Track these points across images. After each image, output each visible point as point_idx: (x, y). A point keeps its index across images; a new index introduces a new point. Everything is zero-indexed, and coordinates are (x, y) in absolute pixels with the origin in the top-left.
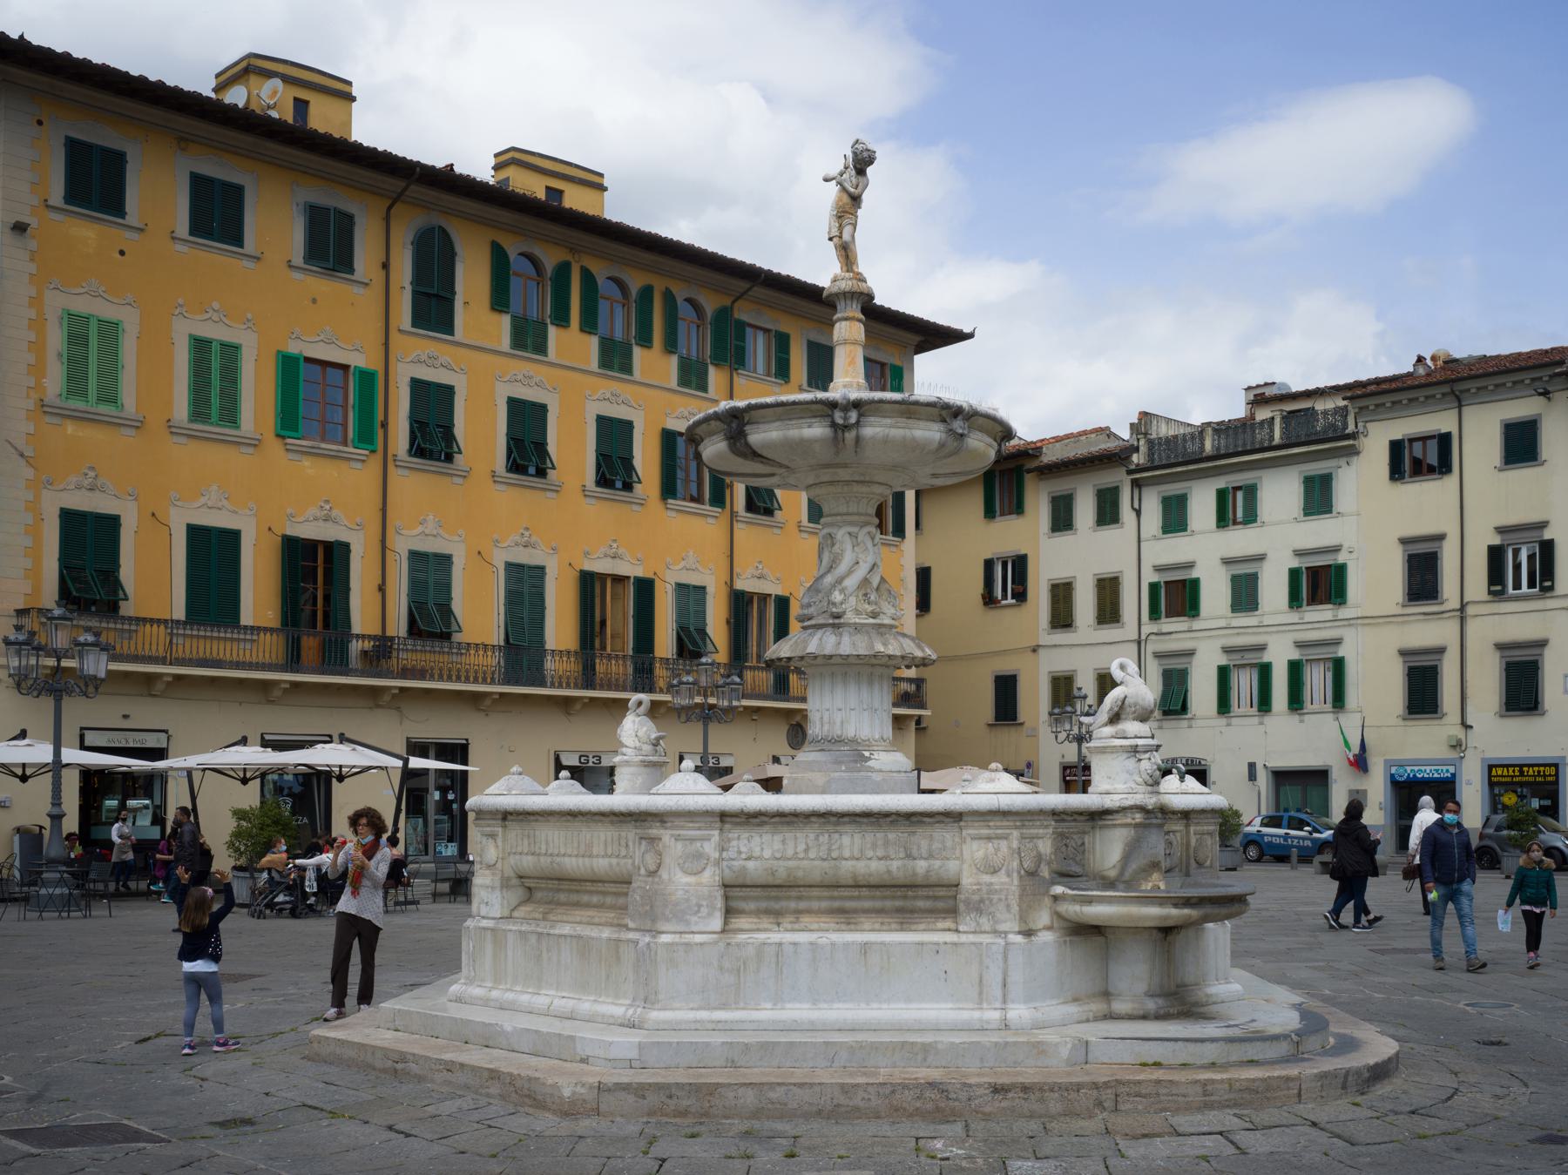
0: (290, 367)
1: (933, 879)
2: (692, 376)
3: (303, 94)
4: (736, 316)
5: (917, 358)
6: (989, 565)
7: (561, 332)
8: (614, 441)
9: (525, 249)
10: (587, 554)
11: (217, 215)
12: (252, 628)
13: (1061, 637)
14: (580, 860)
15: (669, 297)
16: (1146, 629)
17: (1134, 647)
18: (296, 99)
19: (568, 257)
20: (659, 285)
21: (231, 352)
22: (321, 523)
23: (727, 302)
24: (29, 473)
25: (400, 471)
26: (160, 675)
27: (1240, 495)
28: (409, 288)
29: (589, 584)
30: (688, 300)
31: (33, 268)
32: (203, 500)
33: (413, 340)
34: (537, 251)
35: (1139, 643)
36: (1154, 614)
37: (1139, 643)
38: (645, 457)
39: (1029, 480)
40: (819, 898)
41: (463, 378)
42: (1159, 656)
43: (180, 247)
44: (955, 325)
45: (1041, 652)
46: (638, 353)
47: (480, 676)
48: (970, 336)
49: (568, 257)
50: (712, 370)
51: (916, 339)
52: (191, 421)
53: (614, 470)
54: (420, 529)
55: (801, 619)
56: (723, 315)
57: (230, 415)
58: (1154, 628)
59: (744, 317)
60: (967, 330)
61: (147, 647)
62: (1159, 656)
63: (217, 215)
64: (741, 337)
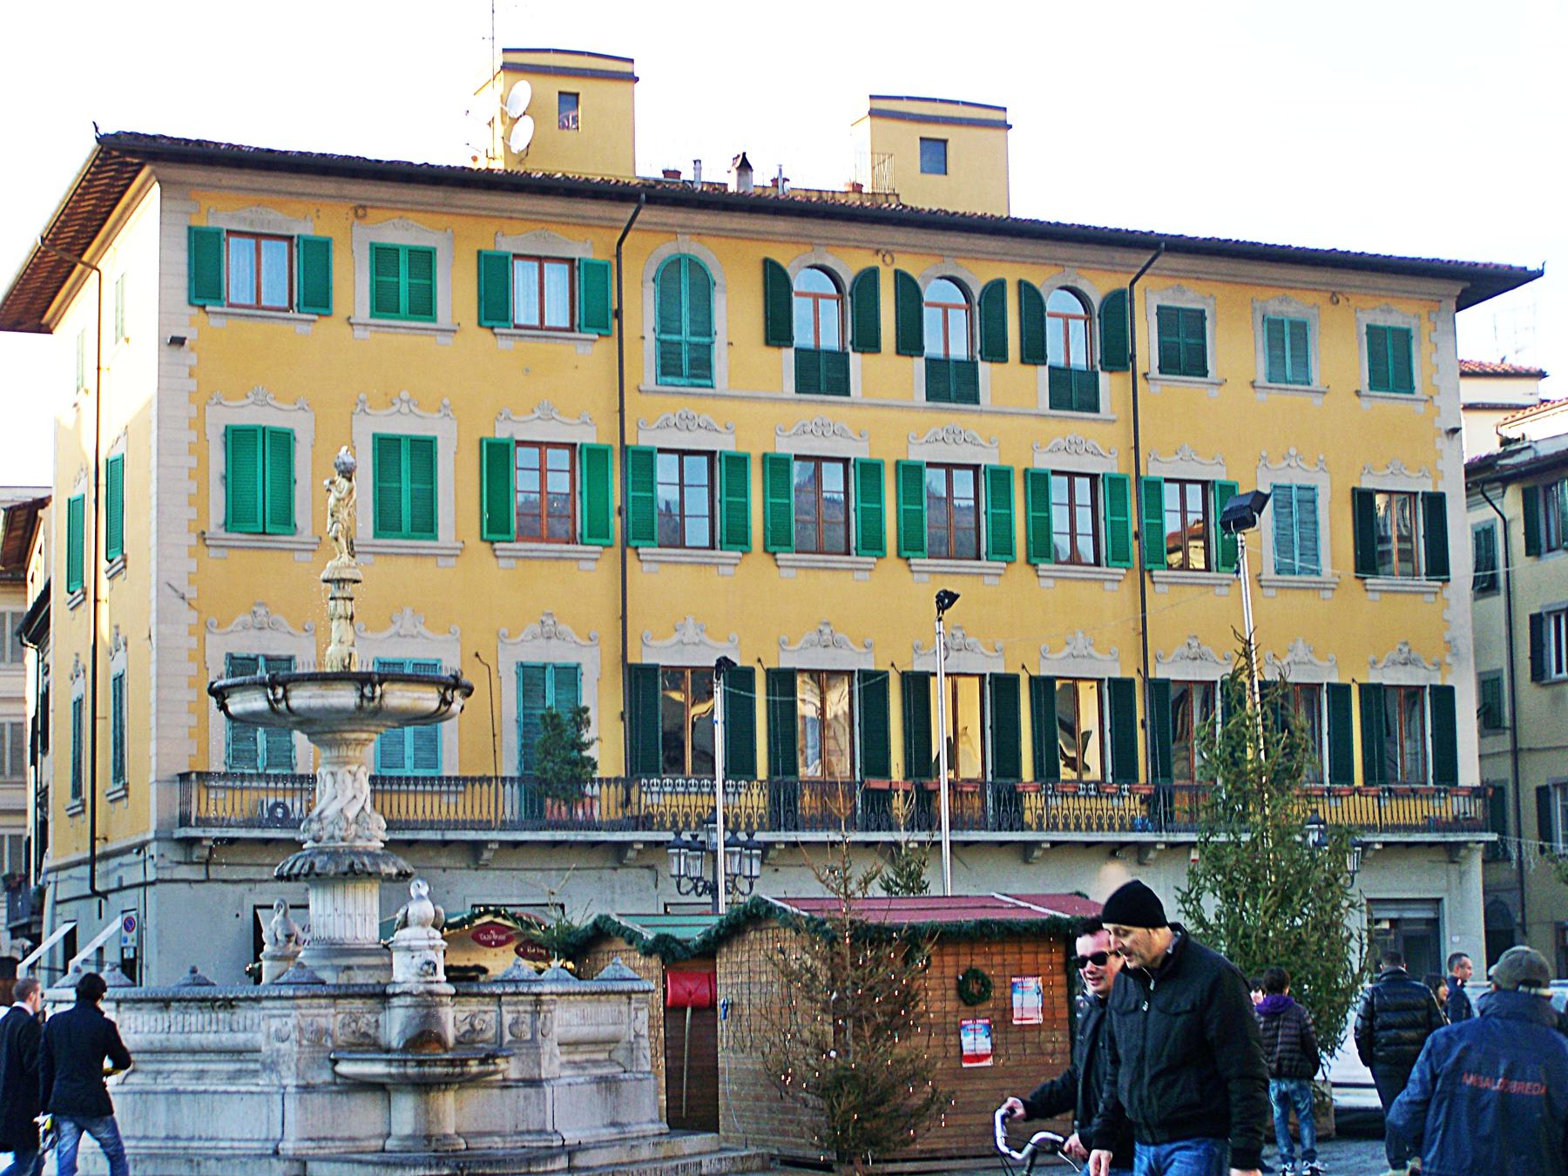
1: (250, 1046)
5: (1458, 315)
7: (996, 366)
8: (404, 464)
10: (916, 649)
11: (1288, 348)
12: (457, 778)
14: (204, 1036)
18: (848, 394)
19: (876, 262)
20: (1011, 274)
21: (425, 449)
22: (254, 632)
23: (1123, 282)
24: (192, 617)
26: (629, 844)
28: (651, 337)
29: (1002, 688)
31: (192, 385)
32: (393, 629)
33: (659, 399)
41: (1326, 476)
44: (1517, 263)
46: (857, 362)
47: (1072, 821)
48: (1540, 274)
49: (876, 262)
50: (1104, 378)
51: (1457, 288)
52: (376, 536)
54: (676, 637)
57: (426, 525)
61: (403, 810)
63: (1288, 348)
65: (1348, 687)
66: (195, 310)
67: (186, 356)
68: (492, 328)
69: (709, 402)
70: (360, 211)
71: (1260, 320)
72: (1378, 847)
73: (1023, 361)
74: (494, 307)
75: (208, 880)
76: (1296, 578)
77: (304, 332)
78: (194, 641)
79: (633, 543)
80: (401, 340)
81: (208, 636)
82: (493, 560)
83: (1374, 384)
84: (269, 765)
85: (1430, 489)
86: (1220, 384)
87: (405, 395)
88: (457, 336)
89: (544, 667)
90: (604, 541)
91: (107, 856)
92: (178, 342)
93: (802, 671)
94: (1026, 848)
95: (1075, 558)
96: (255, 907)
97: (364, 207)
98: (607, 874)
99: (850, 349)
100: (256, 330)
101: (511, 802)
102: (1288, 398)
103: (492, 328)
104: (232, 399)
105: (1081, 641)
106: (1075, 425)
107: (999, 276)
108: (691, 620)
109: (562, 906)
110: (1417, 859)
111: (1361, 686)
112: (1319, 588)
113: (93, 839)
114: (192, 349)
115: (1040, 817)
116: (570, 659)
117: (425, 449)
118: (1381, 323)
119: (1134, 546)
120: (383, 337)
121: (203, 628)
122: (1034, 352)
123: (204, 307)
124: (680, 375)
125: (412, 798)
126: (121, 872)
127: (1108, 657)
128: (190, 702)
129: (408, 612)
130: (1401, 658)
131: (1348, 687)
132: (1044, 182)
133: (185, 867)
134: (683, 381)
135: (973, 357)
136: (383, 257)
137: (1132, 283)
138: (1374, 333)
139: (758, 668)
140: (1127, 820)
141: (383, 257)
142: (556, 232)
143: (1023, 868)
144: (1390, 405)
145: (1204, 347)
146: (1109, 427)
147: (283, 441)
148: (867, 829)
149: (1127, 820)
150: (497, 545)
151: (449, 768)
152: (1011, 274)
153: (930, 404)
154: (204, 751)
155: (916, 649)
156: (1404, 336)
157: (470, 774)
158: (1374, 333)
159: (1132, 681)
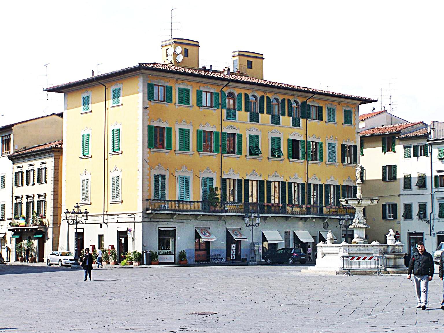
0: (199, 132)
2: (296, 123)
3: (187, 47)
4: (307, 103)
6: (384, 167)
7: (262, 114)
9: (253, 94)
13: (408, 192)
15: (289, 101)
16: (434, 190)
17: (430, 195)
18: (258, 122)
21: (188, 131)
24: (148, 166)
25: (224, 158)
27: (161, 98)
30: (295, 101)
31: (148, 117)
32: (182, 169)
33: (227, 122)
34: (256, 94)
35: (432, 195)
36: (436, 186)
37: (432, 195)
38: (284, 147)
39: (397, 142)
40: (442, 133)
42: (438, 199)
43: (177, 107)
45: (401, 196)
48: (377, 101)
49: (263, 94)
50: (301, 120)
53: (276, 152)
54: (229, 173)
55: (430, 286)
56: (304, 103)
58: (436, 190)
59: (310, 104)
60: (375, 99)
62: (438, 199)
64: (309, 110)
65: (264, 181)
66: (149, 101)
67: (147, 111)
68: (199, 106)
69: (235, 123)
70: (177, 81)
71: (327, 108)
72: (270, 217)
73: (267, 114)
74: (199, 103)
75: (151, 221)
76: (332, 163)
77: (167, 106)
78: (148, 171)
79: (223, 153)
80: (184, 108)
81: (151, 171)
82: (199, 156)
83: (345, 122)
84: (162, 198)
85: (354, 145)
86: (192, 107)
87: (184, 120)
88: (193, 108)
89: (207, 178)
90: (217, 152)
91: (107, 215)
92: (146, 108)
93: (250, 180)
94: (287, 218)
95: (347, 163)
96: (159, 227)
97: (177, 80)
98: (217, 222)
99: (280, 115)
100: (207, 111)
101: (200, 206)
102: (331, 125)
103: (199, 106)
104: (155, 120)
105: (332, 178)
106: (296, 130)
107: (284, 98)
108: (231, 169)
109: (240, 229)
110: (212, 218)
111: (325, 184)
112: (335, 165)
113: (104, 211)
114: (148, 110)
115: (291, 212)
116: (163, 174)
117: (188, 131)
118: (347, 109)
119: (220, 148)
120: (181, 108)
121: (149, 169)
122: (289, 115)
123: (150, 101)
124: (230, 117)
125: (182, 205)
126: (117, 219)
127: (237, 174)
128: (148, 184)
129: (184, 166)
130: (348, 180)
131: (264, 181)
132: (272, 74)
133: (147, 219)
134: (231, 119)
135: (279, 115)
136: (181, 90)
137: (307, 100)
138: (345, 111)
139: (287, 182)
140: (235, 211)
141: (181, 90)
142: (210, 86)
143: (286, 222)
144: (347, 126)
145: (322, 114)
146: (302, 130)
147: (257, 137)
148: (267, 213)
149: (235, 211)
150: (200, 153)
151: (191, 199)
152: (286, 97)
153: (250, 122)
154: (150, 194)
155: (269, 176)
156: (350, 112)
157: (172, 200)
158: (345, 111)
159: (305, 183)
